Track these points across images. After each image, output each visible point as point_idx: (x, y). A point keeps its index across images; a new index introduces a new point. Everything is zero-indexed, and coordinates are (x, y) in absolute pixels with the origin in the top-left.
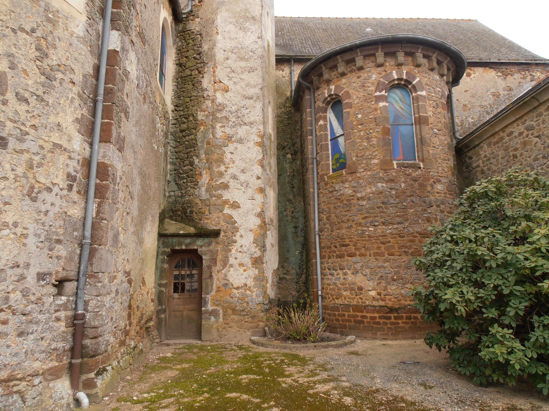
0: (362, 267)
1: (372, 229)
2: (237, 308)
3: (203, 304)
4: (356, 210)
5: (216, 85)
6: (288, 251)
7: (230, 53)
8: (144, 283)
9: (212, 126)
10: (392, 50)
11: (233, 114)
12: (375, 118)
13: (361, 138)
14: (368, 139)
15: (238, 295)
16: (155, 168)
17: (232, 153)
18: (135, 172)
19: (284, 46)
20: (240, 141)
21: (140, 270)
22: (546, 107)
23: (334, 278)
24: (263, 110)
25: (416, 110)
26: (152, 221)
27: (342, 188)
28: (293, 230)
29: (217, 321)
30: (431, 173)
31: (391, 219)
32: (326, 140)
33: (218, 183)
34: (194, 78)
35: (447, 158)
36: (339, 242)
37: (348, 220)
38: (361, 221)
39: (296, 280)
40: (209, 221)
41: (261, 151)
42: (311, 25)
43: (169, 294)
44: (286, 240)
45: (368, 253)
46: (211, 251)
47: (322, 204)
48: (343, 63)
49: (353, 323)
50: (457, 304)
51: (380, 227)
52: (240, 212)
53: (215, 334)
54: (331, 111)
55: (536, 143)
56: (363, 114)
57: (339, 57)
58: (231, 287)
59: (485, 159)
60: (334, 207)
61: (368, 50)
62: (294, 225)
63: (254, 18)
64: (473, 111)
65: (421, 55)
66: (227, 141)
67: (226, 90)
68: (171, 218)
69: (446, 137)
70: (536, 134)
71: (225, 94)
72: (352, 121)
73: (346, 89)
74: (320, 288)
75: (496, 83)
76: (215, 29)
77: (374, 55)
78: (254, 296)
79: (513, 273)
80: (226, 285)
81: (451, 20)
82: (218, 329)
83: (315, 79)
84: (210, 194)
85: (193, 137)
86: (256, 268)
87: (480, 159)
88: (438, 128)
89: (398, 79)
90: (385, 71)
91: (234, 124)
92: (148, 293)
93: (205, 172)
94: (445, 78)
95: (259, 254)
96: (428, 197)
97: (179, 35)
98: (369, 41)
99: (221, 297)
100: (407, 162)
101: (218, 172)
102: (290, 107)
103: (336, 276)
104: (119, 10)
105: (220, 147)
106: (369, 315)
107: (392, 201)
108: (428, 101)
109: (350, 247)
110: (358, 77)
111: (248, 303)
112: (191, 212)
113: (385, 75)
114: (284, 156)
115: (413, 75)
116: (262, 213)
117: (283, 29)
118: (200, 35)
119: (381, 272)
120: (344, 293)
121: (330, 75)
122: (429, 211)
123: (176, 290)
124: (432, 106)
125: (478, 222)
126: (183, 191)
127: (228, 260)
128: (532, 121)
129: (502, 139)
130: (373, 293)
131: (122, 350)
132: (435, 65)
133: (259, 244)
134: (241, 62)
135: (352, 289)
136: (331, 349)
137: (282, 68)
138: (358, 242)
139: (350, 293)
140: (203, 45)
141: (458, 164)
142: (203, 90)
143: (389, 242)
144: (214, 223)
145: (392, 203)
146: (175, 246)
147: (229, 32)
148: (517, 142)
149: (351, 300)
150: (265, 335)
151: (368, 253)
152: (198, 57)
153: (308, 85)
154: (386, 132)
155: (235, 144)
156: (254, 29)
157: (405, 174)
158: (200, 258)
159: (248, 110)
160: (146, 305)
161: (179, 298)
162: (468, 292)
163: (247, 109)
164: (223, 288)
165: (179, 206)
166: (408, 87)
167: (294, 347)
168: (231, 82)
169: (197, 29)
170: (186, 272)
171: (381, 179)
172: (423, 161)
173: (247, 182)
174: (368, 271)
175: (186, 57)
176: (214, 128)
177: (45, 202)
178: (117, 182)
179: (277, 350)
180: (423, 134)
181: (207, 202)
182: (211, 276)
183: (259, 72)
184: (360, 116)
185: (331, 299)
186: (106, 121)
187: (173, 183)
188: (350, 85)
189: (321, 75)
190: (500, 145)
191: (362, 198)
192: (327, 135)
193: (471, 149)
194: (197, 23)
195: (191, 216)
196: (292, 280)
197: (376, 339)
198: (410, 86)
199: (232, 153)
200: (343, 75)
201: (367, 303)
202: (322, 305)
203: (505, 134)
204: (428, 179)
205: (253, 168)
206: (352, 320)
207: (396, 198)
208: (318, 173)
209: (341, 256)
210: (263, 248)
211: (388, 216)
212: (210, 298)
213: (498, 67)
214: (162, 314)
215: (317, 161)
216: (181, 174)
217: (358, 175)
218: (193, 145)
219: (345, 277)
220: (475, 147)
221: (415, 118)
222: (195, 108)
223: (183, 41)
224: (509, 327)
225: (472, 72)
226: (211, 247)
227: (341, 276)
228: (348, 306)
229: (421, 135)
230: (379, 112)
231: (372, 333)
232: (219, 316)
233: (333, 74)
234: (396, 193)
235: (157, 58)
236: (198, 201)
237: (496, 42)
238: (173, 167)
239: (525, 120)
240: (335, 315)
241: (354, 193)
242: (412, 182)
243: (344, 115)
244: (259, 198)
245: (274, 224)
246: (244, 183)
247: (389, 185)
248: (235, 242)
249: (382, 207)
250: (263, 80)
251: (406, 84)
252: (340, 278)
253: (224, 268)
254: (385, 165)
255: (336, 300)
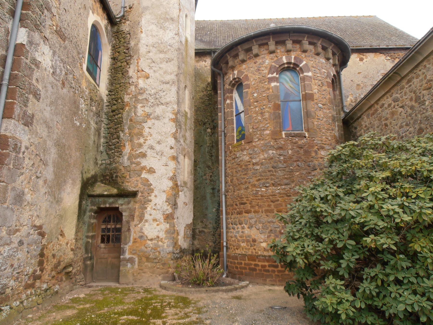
0: (256, 222)
1: (264, 190)
2: (150, 257)
3: (121, 253)
4: (252, 174)
5: (139, 73)
6: (207, 208)
7: (151, 48)
8: (62, 235)
9: (134, 106)
10: (282, 39)
11: (152, 97)
12: (268, 96)
13: (256, 113)
15: (151, 246)
16: (77, 140)
17: (150, 128)
18: (49, 143)
19: (209, 42)
20: (157, 118)
21: (58, 224)
22: (407, 81)
23: (235, 231)
24: (177, 92)
25: (303, 88)
26: (72, 184)
27: (241, 156)
28: (211, 191)
29: (133, 268)
30: (315, 142)
31: (280, 181)
32: (232, 116)
33: (137, 152)
34: (123, 68)
35: (331, 128)
36: (239, 201)
37: (246, 182)
38: (257, 183)
39: (212, 233)
40: (129, 184)
41: (174, 126)
42: (236, 25)
43: (97, 244)
44: (205, 199)
45: (260, 211)
46: (130, 209)
47: (228, 169)
48: (243, 52)
49: (248, 271)
50: (297, 256)
51: (270, 188)
52: (155, 176)
53: (131, 278)
54: (236, 92)
55: (401, 113)
57: (239, 47)
58: (146, 238)
59: (365, 129)
60: (236, 171)
61: (262, 40)
62: (212, 187)
63: (172, 19)
64: (365, 89)
65: (307, 42)
66: (146, 118)
67: (147, 77)
68: (102, 182)
69: (331, 110)
70: (401, 105)
71: (146, 81)
72: (250, 99)
73: (246, 73)
74: (225, 240)
75: (385, 65)
76: (140, 29)
77: (267, 44)
78: (165, 247)
79: (348, 228)
80: (141, 237)
81: (353, 17)
82: (133, 274)
83: (223, 66)
84: (130, 162)
85: (120, 115)
86: (168, 223)
87: (362, 128)
88: (322, 103)
89: (288, 63)
90: (277, 57)
91: (152, 104)
92: (67, 244)
93: (127, 144)
94: (331, 61)
95: (170, 211)
96: (312, 161)
97: (114, 35)
98: (261, 32)
99: (137, 247)
100: (294, 132)
101: (138, 144)
102: (211, 91)
103: (236, 230)
104: (28, 12)
105: (140, 123)
106: (260, 264)
107: (280, 165)
108: (313, 81)
109: (246, 205)
110: (255, 63)
111: (159, 252)
112: (117, 177)
113: (276, 60)
114: (205, 130)
115: (300, 59)
116: (174, 177)
117: (212, 29)
118: (129, 34)
119: (271, 226)
120: (242, 244)
121: (234, 62)
122: (313, 173)
123: (103, 241)
124: (317, 84)
125: (334, 182)
126: (112, 160)
127: (144, 216)
128: (397, 93)
129: (376, 110)
130: (264, 245)
131: (29, 292)
132: (320, 50)
133: (170, 202)
134: (161, 54)
135: (248, 241)
136: (221, 293)
137: (205, 59)
138: (253, 201)
139: (247, 244)
140: (131, 42)
141: (345, 134)
142: (130, 78)
143: (278, 200)
144: (133, 185)
145: (281, 168)
146: (101, 204)
147: (151, 31)
148: (386, 113)
149: (247, 251)
150: (174, 279)
151: (260, 211)
152: (127, 51)
153: (218, 71)
154: (277, 107)
155: (153, 120)
156: (172, 28)
157: (292, 143)
158: (121, 214)
159: (165, 93)
160: (64, 254)
161: (105, 248)
162: (308, 246)
163: (164, 92)
164: (139, 240)
165: (108, 172)
166: (296, 69)
167: (188, 291)
168: (152, 71)
169: (127, 29)
170: (111, 226)
171: (272, 147)
172: (308, 131)
173: (162, 151)
174: (260, 226)
175: (118, 52)
176: (135, 108)
178: (22, 151)
179: (175, 293)
180: (308, 109)
181: (128, 169)
182: (129, 230)
183: (175, 62)
184: (255, 95)
185: (233, 249)
186: (10, 101)
187: (105, 153)
188: (248, 70)
189: (227, 63)
190: (375, 115)
191: (256, 164)
192: (232, 111)
193: (355, 121)
194: (127, 25)
195: (116, 180)
196: (209, 233)
197: (266, 284)
198: (298, 69)
199: (150, 128)
200: (243, 61)
202: (226, 254)
203: (379, 107)
204: (313, 147)
205: (167, 140)
206: (248, 267)
207: (284, 163)
208: (225, 144)
209: (240, 213)
210: (175, 205)
211: (277, 178)
212: (128, 248)
213: (387, 52)
214: (88, 261)
215: (225, 133)
216: (110, 146)
217: (254, 144)
218: (120, 122)
219: (243, 230)
220: (358, 119)
221: (302, 94)
222: (123, 92)
223: (117, 40)
224: (342, 278)
225: (364, 57)
226: (130, 206)
227: (240, 230)
228: (244, 256)
229: (307, 109)
230: (271, 90)
231: (263, 280)
232: (134, 263)
233: (236, 61)
234: (284, 159)
235: (84, 53)
236: (121, 167)
237: (388, 32)
238: (105, 140)
239: (392, 93)
240: (235, 263)
241: (250, 160)
242: (298, 149)
243: (244, 94)
244: (172, 164)
245: (188, 186)
246: (159, 152)
247: (278, 152)
248: (151, 201)
249: (272, 171)
250: (179, 68)
251: (295, 67)
252: (239, 231)
253: (140, 222)
254: (276, 135)
255: (236, 250)
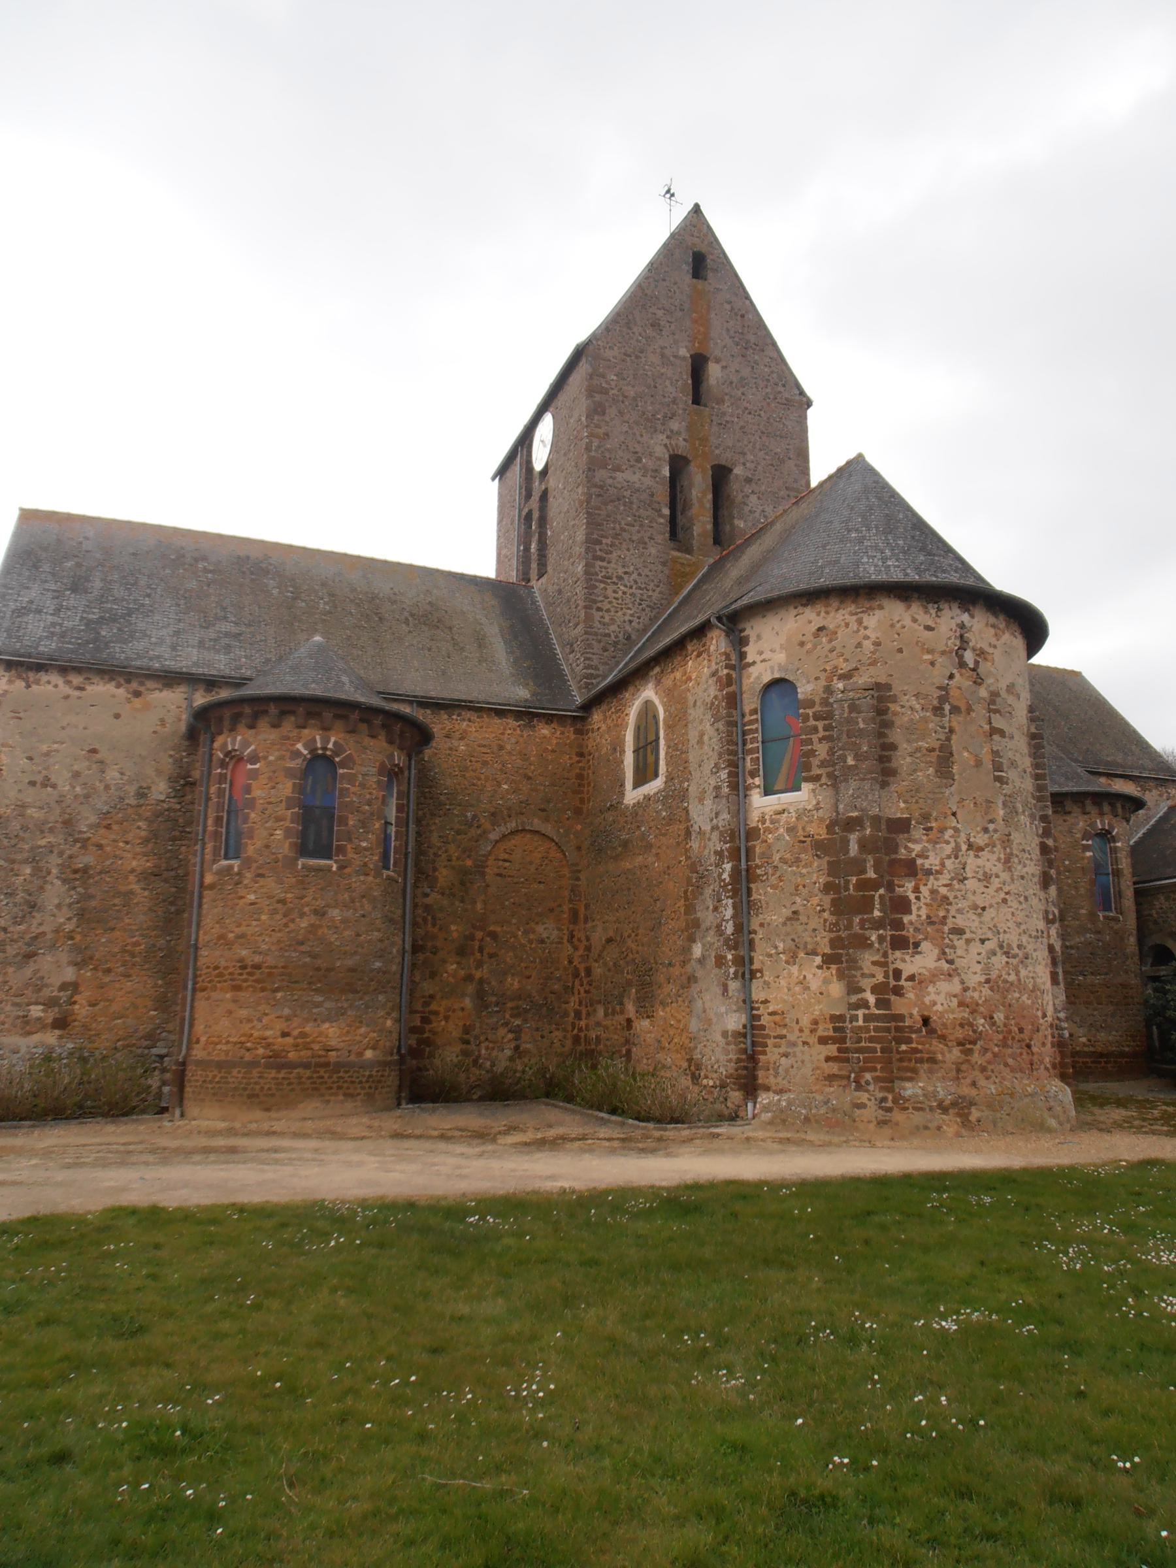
13: (1069, 885)
14: (1076, 888)
38: (1071, 969)
56: (1070, 861)
106: (1081, 1060)
110: (1065, 821)
130: (1083, 1040)
172: (1121, 914)
177: (668, 196)
201: (1078, 1049)
